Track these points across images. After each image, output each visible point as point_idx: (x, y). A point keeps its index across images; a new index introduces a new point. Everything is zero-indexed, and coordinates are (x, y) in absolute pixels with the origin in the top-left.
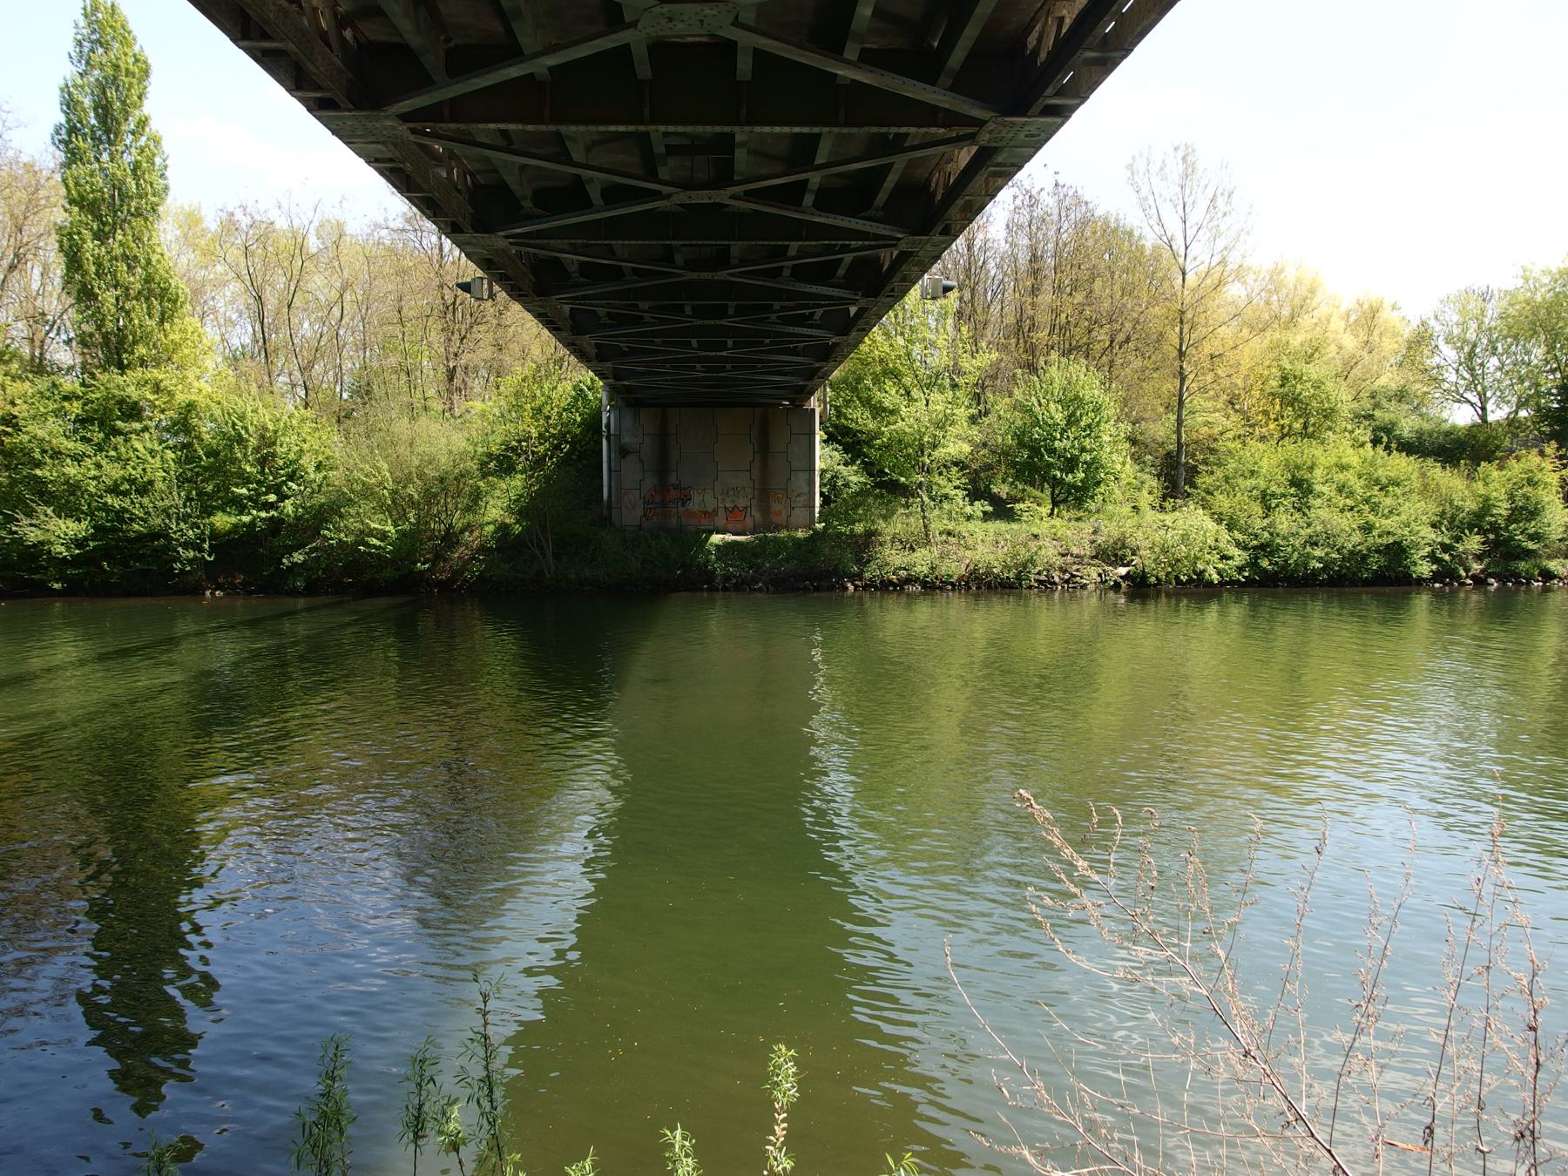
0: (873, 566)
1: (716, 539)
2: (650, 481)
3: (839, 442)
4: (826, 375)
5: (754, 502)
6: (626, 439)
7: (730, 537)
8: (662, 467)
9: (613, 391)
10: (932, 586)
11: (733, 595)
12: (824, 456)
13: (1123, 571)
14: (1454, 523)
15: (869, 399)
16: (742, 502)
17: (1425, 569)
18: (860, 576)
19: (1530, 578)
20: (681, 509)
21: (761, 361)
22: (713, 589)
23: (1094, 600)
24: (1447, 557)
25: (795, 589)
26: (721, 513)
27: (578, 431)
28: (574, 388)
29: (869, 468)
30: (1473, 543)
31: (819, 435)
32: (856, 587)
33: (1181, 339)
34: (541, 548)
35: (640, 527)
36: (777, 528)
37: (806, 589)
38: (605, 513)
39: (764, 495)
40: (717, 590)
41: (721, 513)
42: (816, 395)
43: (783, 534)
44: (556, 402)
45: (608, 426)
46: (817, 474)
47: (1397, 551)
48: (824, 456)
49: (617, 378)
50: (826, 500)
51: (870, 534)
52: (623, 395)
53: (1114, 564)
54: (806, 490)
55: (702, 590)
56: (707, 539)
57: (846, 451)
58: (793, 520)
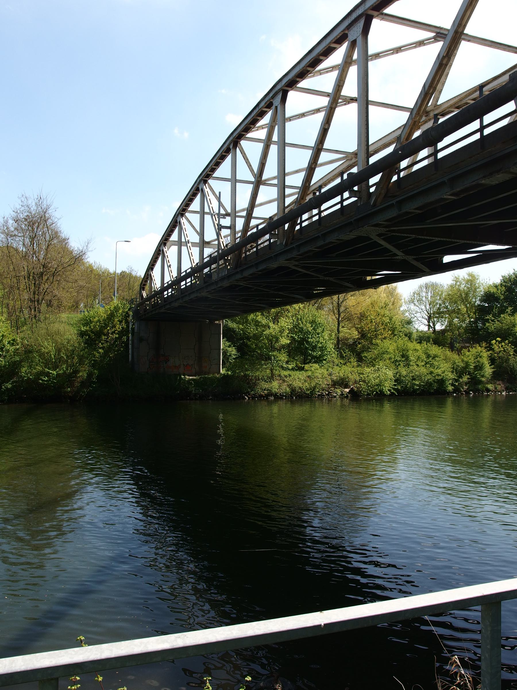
10: (278, 397)
12: (223, 344)
13: (347, 390)
14: (460, 372)
17: (450, 388)
19: (483, 392)
23: (465, 398)
24: (457, 384)
30: (465, 378)
32: (249, 398)
33: (339, 299)
36: (209, 373)
47: (442, 382)
48: (223, 344)
53: (346, 388)
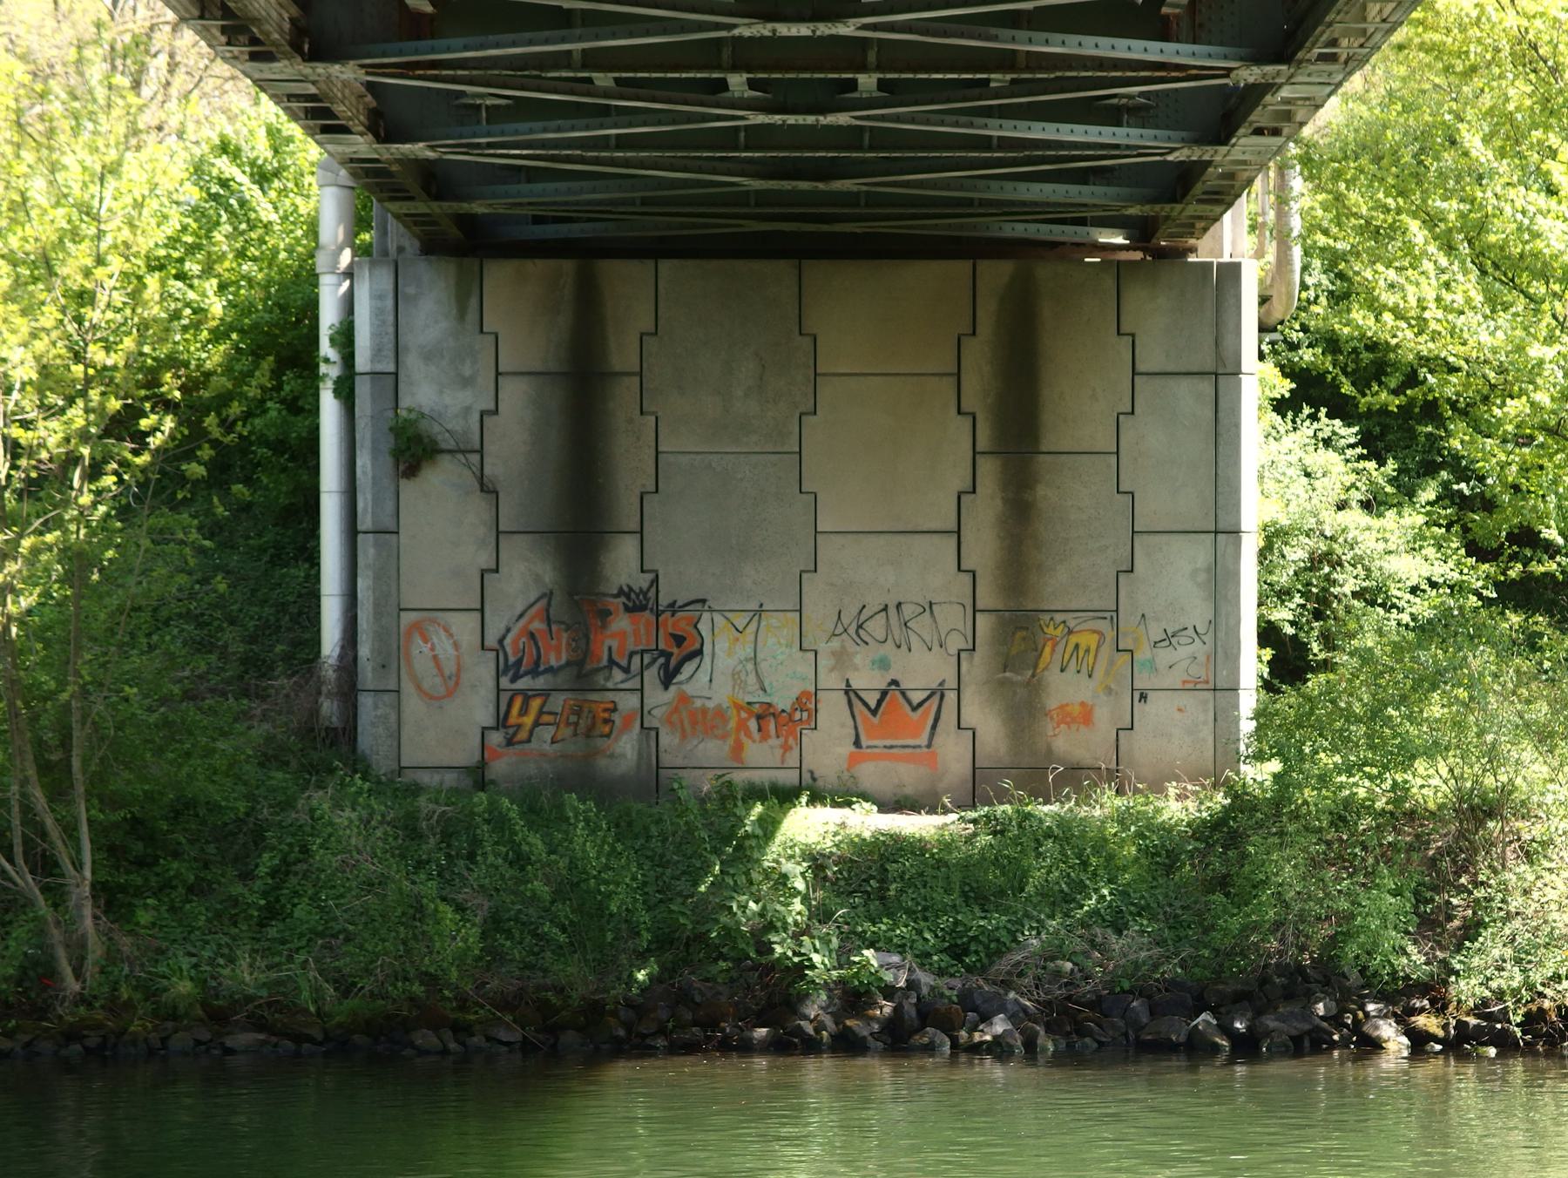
0: (1493, 946)
1: (808, 826)
2: (526, 575)
3: (1342, 409)
4: (1283, 124)
5: (976, 669)
6: (426, 393)
7: (865, 821)
8: (579, 513)
9: (373, 184)
11: (880, 1071)
12: (1289, 475)
15: (1475, 229)
16: (922, 669)
18: (1434, 992)
20: (658, 698)
21: (1007, 61)
22: (792, 1044)
25: (1160, 1048)
26: (833, 711)
27: (214, 357)
28: (198, 170)
29: (1473, 519)
31: (1260, 380)
32: (1419, 1041)
34: (44, 865)
35: (478, 776)
36: (1077, 778)
37: (1196, 1050)
38: (329, 708)
39: (1018, 634)
40: (811, 1047)
41: (833, 711)
42: (1245, 207)
43: (1104, 806)
44: (116, 232)
45: (345, 337)
46: (1251, 544)
49: (384, 126)
50: (1288, 662)
51: (1479, 810)
52: (436, 216)
54: (1198, 613)
55: (747, 1048)
56: (769, 827)
57: (1374, 446)
58: (1141, 746)
